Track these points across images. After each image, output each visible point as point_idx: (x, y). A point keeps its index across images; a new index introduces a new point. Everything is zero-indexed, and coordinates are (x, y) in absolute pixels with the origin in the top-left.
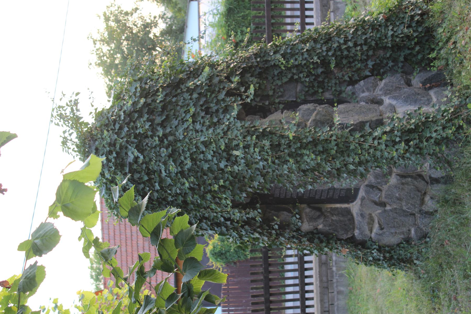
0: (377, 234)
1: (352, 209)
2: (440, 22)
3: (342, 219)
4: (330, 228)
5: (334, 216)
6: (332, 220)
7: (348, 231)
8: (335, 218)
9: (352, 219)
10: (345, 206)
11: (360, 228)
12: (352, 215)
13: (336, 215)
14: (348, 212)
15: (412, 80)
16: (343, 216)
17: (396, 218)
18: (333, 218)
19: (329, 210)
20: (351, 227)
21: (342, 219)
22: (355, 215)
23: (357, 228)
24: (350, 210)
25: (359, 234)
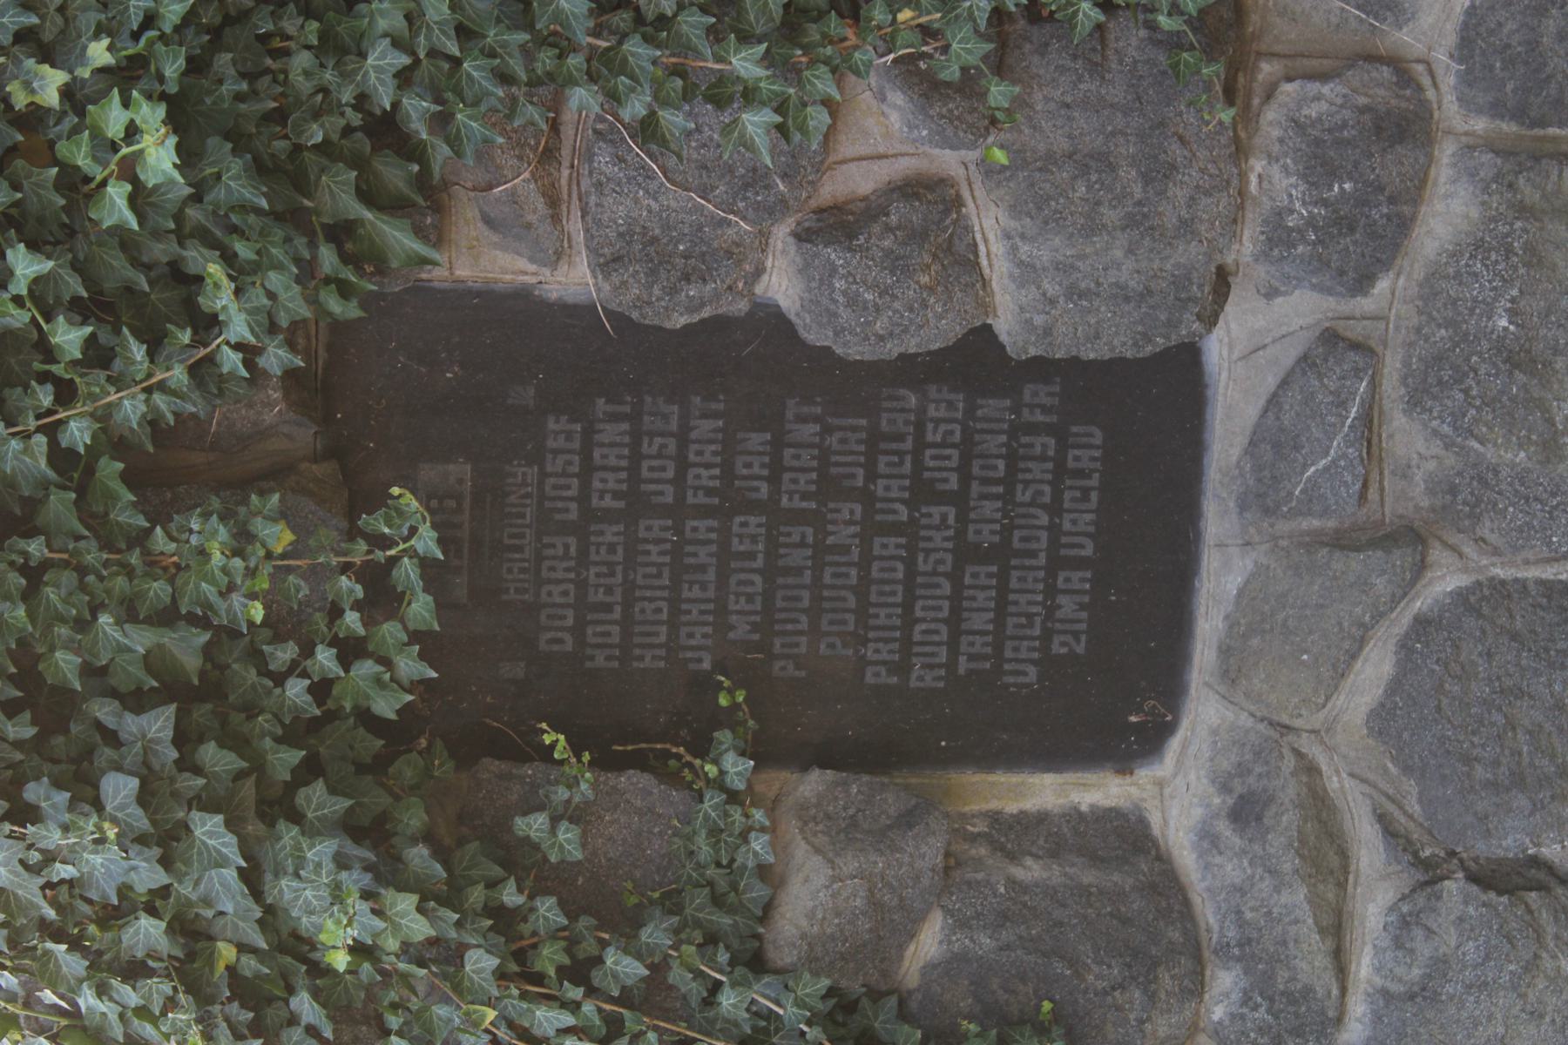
0: (1385, 993)
1: (1155, 820)
2: (1288, 87)
3: (1089, 877)
4: (1006, 935)
5: (1029, 861)
6: (1012, 882)
7: (1155, 964)
8: (1031, 871)
9: (1166, 887)
10: (1098, 790)
11: (1245, 942)
12: (1164, 861)
13: (1036, 857)
14: (1128, 837)
15: (489, 971)
16: (1096, 860)
17: (1520, 693)
18: (1018, 873)
19: (980, 827)
20: (1175, 935)
21: (1089, 877)
22: (1186, 859)
23: (1222, 950)
24: (1143, 822)
25: (1246, 1000)
